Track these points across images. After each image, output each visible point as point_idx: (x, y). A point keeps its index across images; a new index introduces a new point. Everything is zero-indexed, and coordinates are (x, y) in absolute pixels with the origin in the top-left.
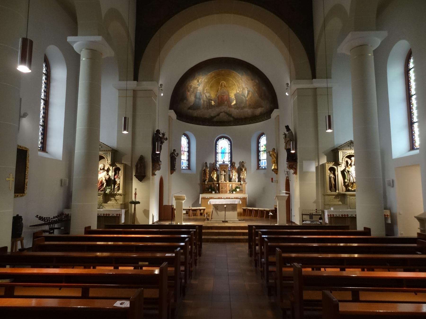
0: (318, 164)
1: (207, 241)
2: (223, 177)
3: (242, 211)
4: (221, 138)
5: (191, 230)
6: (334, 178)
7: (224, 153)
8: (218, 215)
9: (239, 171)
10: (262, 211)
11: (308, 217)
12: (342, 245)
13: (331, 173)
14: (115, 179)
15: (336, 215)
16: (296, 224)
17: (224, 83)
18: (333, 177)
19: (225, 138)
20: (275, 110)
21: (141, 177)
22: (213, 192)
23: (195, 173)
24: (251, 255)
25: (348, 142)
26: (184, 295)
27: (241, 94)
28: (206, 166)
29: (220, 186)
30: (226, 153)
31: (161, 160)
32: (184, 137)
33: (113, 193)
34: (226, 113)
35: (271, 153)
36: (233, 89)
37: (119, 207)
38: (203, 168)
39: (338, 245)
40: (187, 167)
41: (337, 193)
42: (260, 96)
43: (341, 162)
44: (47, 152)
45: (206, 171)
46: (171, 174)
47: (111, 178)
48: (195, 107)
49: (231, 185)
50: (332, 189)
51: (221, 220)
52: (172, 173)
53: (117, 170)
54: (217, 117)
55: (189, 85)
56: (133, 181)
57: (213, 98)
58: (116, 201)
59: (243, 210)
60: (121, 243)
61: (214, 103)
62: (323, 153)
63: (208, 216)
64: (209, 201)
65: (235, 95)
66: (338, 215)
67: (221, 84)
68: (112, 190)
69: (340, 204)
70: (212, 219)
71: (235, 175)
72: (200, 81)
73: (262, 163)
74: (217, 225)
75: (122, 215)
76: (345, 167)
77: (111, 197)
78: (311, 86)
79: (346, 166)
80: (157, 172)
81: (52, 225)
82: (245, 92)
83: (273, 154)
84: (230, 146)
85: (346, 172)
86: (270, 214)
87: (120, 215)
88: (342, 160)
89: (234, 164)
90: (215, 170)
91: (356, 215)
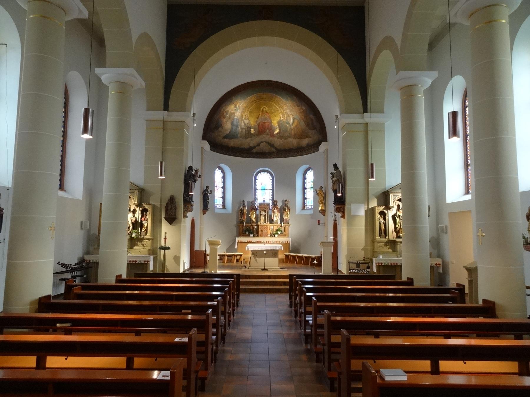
0: (368, 207)
1: (245, 291)
2: (263, 218)
3: (284, 257)
4: (261, 171)
5: (228, 279)
6: (384, 223)
7: (264, 189)
8: (257, 262)
9: (282, 211)
10: (307, 258)
11: (354, 266)
12: (391, 295)
13: (381, 218)
14: (141, 221)
15: (385, 264)
16: (343, 273)
17: (266, 109)
18: (383, 221)
19: (266, 172)
20: (323, 143)
21: (172, 219)
22: (251, 235)
23: (231, 213)
24: (291, 306)
25: (400, 185)
26: (224, 343)
27: (285, 121)
28: (243, 204)
29: (259, 228)
30: (266, 189)
31: (193, 201)
32: (218, 170)
33: (140, 237)
34: (267, 143)
35: (318, 192)
36: (276, 116)
37: (147, 253)
38: (240, 207)
39: (387, 295)
40: (221, 206)
41: (387, 240)
42: (308, 125)
43: (392, 206)
44: (65, 191)
45: (244, 211)
46: (204, 214)
47: (138, 220)
48: (231, 136)
49: (272, 227)
50: (381, 235)
51: (261, 267)
52: (204, 213)
53: (144, 212)
54: (257, 148)
55: (225, 110)
56: (162, 224)
57: (253, 125)
58: (144, 246)
59: (285, 256)
60: (148, 292)
61: (254, 132)
62: (373, 195)
63: (246, 263)
64: (247, 247)
65: (279, 122)
66: (386, 264)
67: (262, 109)
68: (139, 233)
69: (390, 252)
70: (250, 266)
71: (277, 216)
72: (237, 106)
73: (308, 202)
74: (255, 273)
75: (150, 262)
76: (396, 212)
77: (138, 242)
78: (361, 121)
79: (397, 210)
80: (189, 214)
81: (74, 273)
82: (290, 120)
83: (321, 194)
84: (272, 181)
85: (397, 217)
86: (314, 262)
87: (148, 262)
88: (393, 204)
89: (275, 203)
90: (254, 209)
91: (401, 264)
